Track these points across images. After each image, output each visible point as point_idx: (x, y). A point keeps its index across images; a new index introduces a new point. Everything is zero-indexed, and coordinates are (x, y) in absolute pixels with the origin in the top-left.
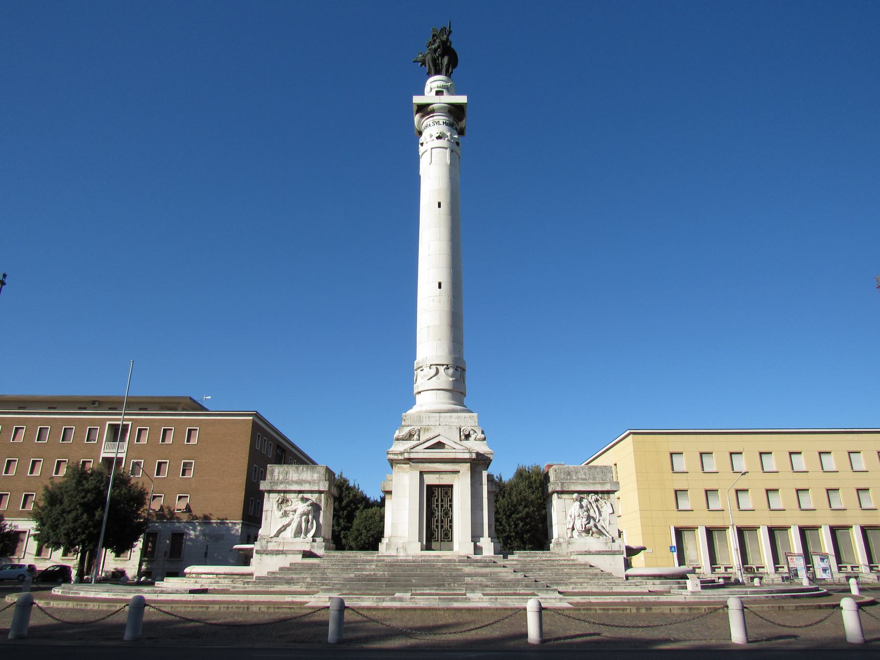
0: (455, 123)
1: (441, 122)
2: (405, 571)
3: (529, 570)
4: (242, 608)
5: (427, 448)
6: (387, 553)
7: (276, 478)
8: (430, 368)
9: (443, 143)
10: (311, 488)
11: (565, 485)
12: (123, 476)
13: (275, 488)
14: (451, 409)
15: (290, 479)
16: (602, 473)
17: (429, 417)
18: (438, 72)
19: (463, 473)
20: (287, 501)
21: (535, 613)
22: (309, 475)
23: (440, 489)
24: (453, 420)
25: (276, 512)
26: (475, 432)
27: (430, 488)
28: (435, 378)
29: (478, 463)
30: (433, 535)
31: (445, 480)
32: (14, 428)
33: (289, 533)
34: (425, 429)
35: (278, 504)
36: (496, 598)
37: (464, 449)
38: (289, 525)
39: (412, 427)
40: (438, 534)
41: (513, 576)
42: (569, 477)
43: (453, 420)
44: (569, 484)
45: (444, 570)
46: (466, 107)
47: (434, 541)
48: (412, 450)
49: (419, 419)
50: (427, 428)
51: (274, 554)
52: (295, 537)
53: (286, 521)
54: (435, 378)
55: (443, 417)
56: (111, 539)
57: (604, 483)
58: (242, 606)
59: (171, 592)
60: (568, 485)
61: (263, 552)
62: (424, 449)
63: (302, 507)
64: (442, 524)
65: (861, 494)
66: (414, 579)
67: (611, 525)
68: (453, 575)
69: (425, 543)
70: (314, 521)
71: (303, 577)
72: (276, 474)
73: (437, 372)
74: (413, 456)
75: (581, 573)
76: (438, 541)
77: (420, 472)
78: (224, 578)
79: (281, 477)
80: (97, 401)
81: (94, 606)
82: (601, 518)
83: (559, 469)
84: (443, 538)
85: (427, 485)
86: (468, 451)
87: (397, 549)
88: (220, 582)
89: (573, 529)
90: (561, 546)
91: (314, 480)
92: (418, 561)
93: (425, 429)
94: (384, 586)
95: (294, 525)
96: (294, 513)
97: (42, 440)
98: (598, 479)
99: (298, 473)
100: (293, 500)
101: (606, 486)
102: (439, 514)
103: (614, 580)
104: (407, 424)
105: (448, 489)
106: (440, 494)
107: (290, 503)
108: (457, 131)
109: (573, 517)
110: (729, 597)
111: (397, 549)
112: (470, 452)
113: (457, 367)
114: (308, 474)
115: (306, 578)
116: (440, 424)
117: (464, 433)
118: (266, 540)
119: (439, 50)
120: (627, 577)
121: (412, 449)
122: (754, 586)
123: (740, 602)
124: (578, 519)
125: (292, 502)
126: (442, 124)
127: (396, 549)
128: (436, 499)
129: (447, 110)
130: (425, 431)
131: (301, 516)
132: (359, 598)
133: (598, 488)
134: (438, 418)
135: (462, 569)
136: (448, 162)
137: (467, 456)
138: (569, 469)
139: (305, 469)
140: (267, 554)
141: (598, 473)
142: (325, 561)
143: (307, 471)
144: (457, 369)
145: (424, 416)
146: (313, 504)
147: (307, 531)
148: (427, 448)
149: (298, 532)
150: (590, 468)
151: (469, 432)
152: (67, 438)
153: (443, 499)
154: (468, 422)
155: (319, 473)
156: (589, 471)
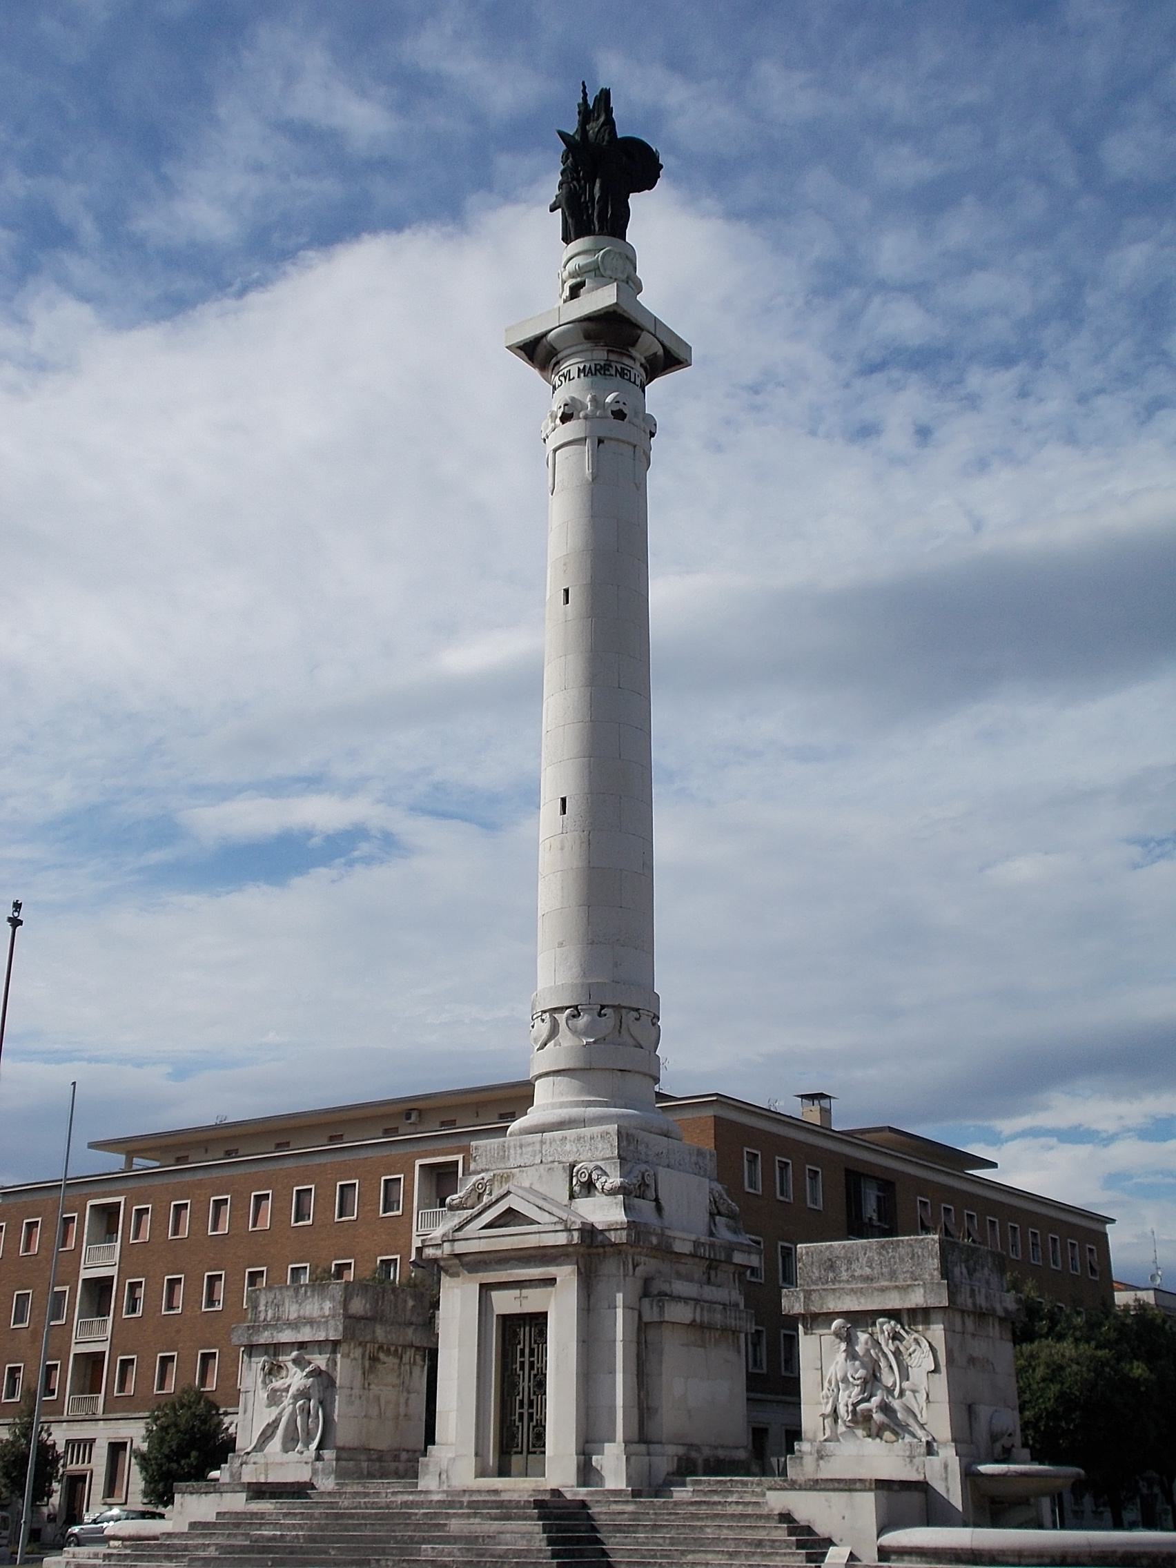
1: (574, 373)
3: (631, 1529)
5: (488, 1226)
7: (262, 1318)
9: (573, 429)
11: (814, 1296)
12: (596, 1276)
14: (567, 1117)
17: (521, 1146)
19: (561, 1281)
23: (527, 1329)
24: (568, 1147)
25: (260, 1391)
26: (605, 1174)
27: (510, 1324)
30: (514, 1436)
31: (530, 1302)
32: (417, 1168)
35: (265, 1375)
40: (524, 1434)
41: (525, 1543)
42: (831, 1275)
44: (823, 1293)
45: (413, 1528)
47: (516, 1453)
48: (460, 1235)
49: (501, 1153)
50: (505, 1175)
53: (274, 1412)
54: (550, 1045)
55: (548, 1142)
56: (1061, 1441)
60: (821, 1298)
64: (531, 1411)
66: (333, 1548)
67: (932, 1405)
68: (416, 1539)
73: (554, 1032)
74: (460, 1248)
75: (727, 1539)
77: (481, 1285)
80: (414, 1109)
82: (906, 1384)
83: (807, 1253)
84: (534, 1446)
90: (802, 1465)
97: (348, 1214)
98: (901, 1277)
99: (297, 1301)
102: (525, 1385)
103: (784, 1559)
104: (479, 1169)
105: (538, 1321)
107: (284, 1373)
112: (570, 1230)
113: (603, 1007)
116: (541, 1162)
117: (578, 1180)
120: (885, 1554)
124: (844, 1391)
127: (438, 1473)
128: (521, 1349)
129: (582, 335)
133: (894, 1301)
134: (537, 1147)
135: (445, 1525)
136: (588, 472)
137: (562, 1239)
138: (831, 1253)
139: (309, 1294)
140: (192, 1493)
141: (902, 1260)
142: (284, 1505)
143: (313, 1296)
146: (317, 1373)
151: (590, 1175)
152: (348, 1210)
153: (534, 1349)
155: (333, 1299)
156: (880, 1254)
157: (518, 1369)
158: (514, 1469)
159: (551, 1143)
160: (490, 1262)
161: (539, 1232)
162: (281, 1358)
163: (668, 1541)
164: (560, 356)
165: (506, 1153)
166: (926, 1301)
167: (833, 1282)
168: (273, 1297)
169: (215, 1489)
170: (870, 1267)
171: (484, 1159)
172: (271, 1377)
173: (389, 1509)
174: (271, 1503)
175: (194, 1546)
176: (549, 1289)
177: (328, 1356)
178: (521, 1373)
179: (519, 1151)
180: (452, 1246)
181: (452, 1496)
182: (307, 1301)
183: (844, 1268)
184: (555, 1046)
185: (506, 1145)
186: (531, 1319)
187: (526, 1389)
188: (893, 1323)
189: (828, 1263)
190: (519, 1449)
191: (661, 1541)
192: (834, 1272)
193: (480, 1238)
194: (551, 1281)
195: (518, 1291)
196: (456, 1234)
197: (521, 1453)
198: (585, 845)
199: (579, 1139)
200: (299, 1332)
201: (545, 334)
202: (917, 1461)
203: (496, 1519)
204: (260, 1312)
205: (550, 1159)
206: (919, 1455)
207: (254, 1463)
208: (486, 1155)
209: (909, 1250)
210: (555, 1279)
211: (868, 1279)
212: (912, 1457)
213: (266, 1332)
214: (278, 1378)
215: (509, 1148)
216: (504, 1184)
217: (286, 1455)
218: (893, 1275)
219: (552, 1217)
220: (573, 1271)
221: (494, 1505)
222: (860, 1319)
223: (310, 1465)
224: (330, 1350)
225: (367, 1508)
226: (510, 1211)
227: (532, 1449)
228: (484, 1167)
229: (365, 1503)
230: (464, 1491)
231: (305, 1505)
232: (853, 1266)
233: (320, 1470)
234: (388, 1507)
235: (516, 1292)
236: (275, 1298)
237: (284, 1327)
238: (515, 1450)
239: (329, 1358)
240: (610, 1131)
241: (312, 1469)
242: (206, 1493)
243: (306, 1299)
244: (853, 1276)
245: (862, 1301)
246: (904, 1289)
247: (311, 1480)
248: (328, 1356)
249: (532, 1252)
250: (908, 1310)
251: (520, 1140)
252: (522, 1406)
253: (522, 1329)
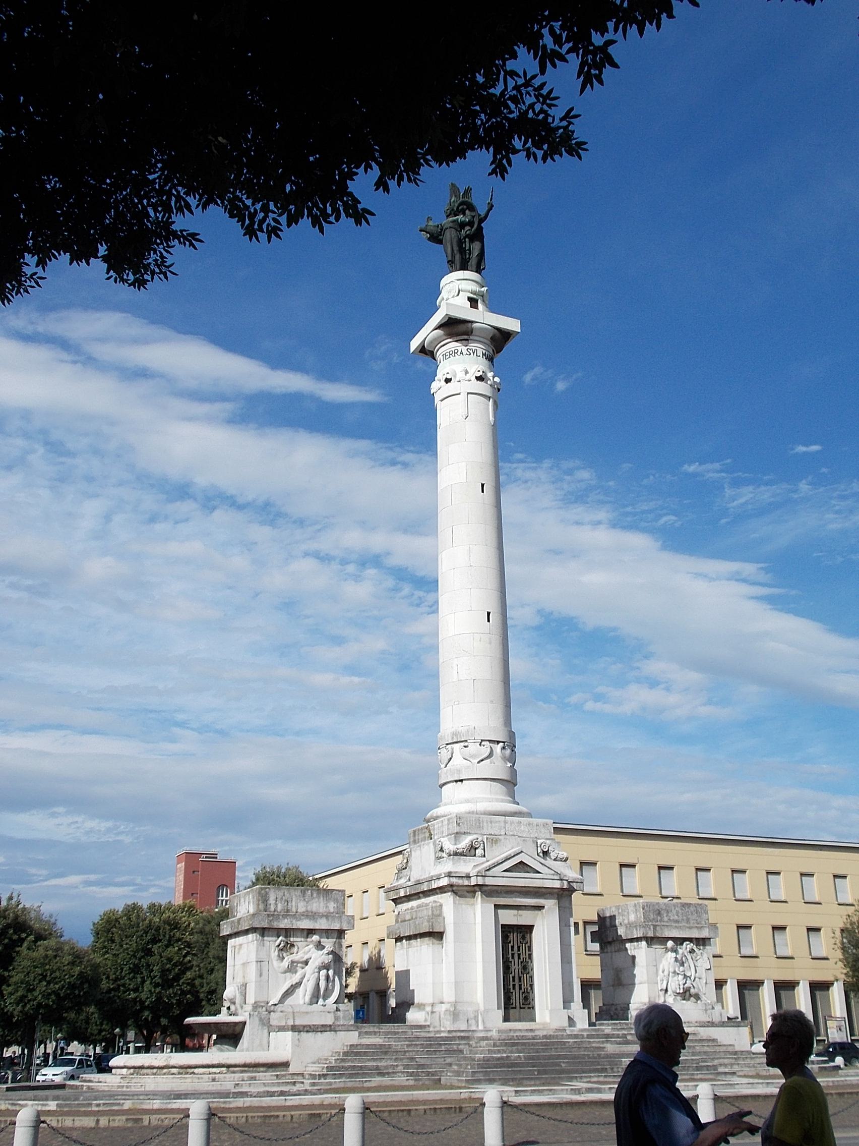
1: (480, 353)
2: (537, 1052)
4: (453, 1109)
5: (539, 872)
6: (455, 1026)
7: (272, 908)
8: (480, 745)
9: (482, 387)
10: (329, 925)
11: (658, 928)
13: (276, 925)
15: (294, 910)
16: (697, 913)
18: (464, 267)
20: (292, 945)
21: (711, 1100)
22: (322, 904)
23: (515, 934)
24: (522, 828)
28: (489, 760)
29: (562, 894)
33: (302, 996)
34: (492, 840)
36: (285, 1099)
37: (553, 875)
38: (299, 984)
39: (475, 836)
40: (517, 997)
42: (659, 918)
43: (522, 828)
44: (663, 927)
45: (583, 1049)
46: (514, 337)
47: (512, 1008)
48: (488, 873)
49: (478, 824)
50: (495, 839)
51: (318, 1032)
52: (311, 1004)
53: (296, 978)
55: (509, 822)
57: (702, 927)
58: (245, 1115)
59: (297, 1092)
61: (301, 1029)
62: (504, 871)
63: (319, 957)
65: (742, 931)
66: (564, 1062)
68: (602, 1056)
70: (336, 978)
71: (392, 1065)
72: (272, 901)
73: (490, 755)
74: (489, 881)
75: (720, 1052)
76: (515, 1008)
78: (242, 1072)
79: (279, 908)
81: (74, 1120)
83: (647, 906)
84: (523, 1004)
85: (502, 925)
86: (558, 878)
87: (468, 1021)
88: (257, 1078)
89: (666, 991)
91: (330, 913)
92: (538, 1037)
93: (492, 840)
94: (536, 1073)
95: (308, 987)
96: (303, 966)
100: (300, 944)
101: (703, 932)
102: (515, 967)
106: (515, 939)
107: (295, 950)
109: (666, 973)
110: (348, 1097)
111: (468, 1021)
112: (561, 880)
114: (320, 903)
115: (397, 1066)
118: (264, 1009)
119: (467, 228)
121: (488, 870)
122: (535, 1075)
123: (207, 1108)
125: (298, 948)
126: (481, 356)
130: (492, 843)
131: (320, 969)
132: (550, 1090)
133: (695, 934)
134: (502, 824)
135: (604, 1048)
137: (557, 884)
139: (315, 895)
140: (307, 1031)
141: (692, 914)
142: (391, 1039)
144: (483, 743)
145: (485, 819)
147: (326, 997)
148: (539, 872)
149: (316, 996)
150: (683, 906)
154: (540, 832)
156: (682, 909)
157: (510, 958)
158: (511, 1017)
159: (511, 824)
160: (501, 892)
161: (543, 879)
162: (292, 939)
163: (691, 1054)
164: (471, 337)
165: (481, 825)
166: (709, 935)
167: (661, 921)
168: (282, 895)
169: (331, 1029)
170: (677, 915)
171: (465, 826)
172: (283, 952)
173: (534, 1039)
174: (380, 1038)
175: (385, 1067)
176: (536, 912)
177: (335, 940)
178: (513, 960)
179: (490, 825)
180: (484, 879)
181: (502, 1033)
182: (314, 901)
183: (665, 915)
184: (491, 763)
185: (481, 819)
186: (518, 928)
187: (517, 970)
188: (692, 944)
189: (657, 912)
190: (514, 1006)
191: (687, 1054)
192: (660, 916)
193: (503, 877)
194: (540, 908)
195: (516, 911)
196: (487, 872)
197: (515, 1008)
198: (501, 646)
199: (529, 824)
200: (316, 922)
201: (472, 322)
202: (709, 1012)
203: (620, 1044)
204: (270, 905)
205: (511, 833)
206: (709, 1009)
207: (282, 1012)
208: (467, 824)
209: (695, 909)
210: (544, 907)
211: (677, 921)
212: (706, 1010)
213: (286, 920)
214: (288, 953)
215: (483, 822)
216: (494, 844)
217: (311, 1006)
218: (688, 921)
219: (550, 870)
220: (555, 904)
221: (604, 1036)
222: (680, 941)
223: (332, 1014)
224: (336, 936)
225: (519, 1039)
226: (521, 863)
227: (522, 1006)
228: (466, 831)
229: (517, 1036)
230: (510, 1030)
231: (408, 1039)
232: (670, 915)
233: (341, 1017)
234: (534, 1039)
235: (515, 912)
236: (284, 895)
237: (302, 917)
238: (511, 1006)
239: (335, 942)
240: (548, 823)
241: (335, 1017)
242: (321, 1031)
243: (312, 899)
244: (669, 919)
245: (681, 932)
246: (700, 928)
247: (286, 1023)
248: (335, 940)
249: (532, 889)
250: (696, 938)
251: (490, 818)
252: (514, 981)
253: (512, 934)
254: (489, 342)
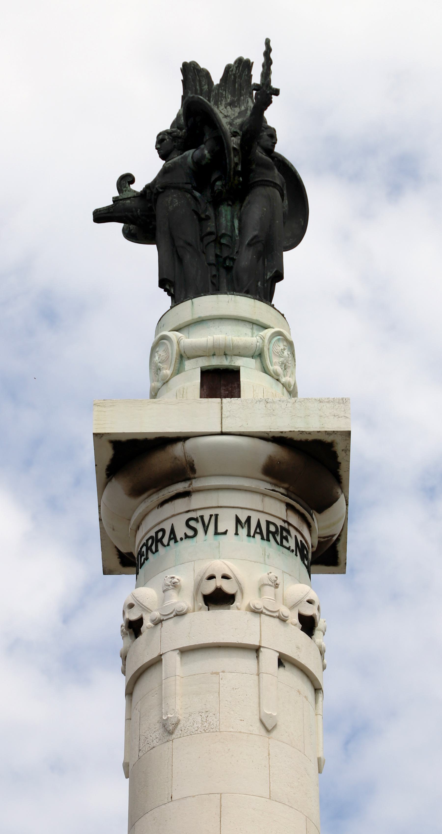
0: (294, 520)
69: (266, 260)
108: (303, 557)
164: (197, 484)
254: (264, 486)
